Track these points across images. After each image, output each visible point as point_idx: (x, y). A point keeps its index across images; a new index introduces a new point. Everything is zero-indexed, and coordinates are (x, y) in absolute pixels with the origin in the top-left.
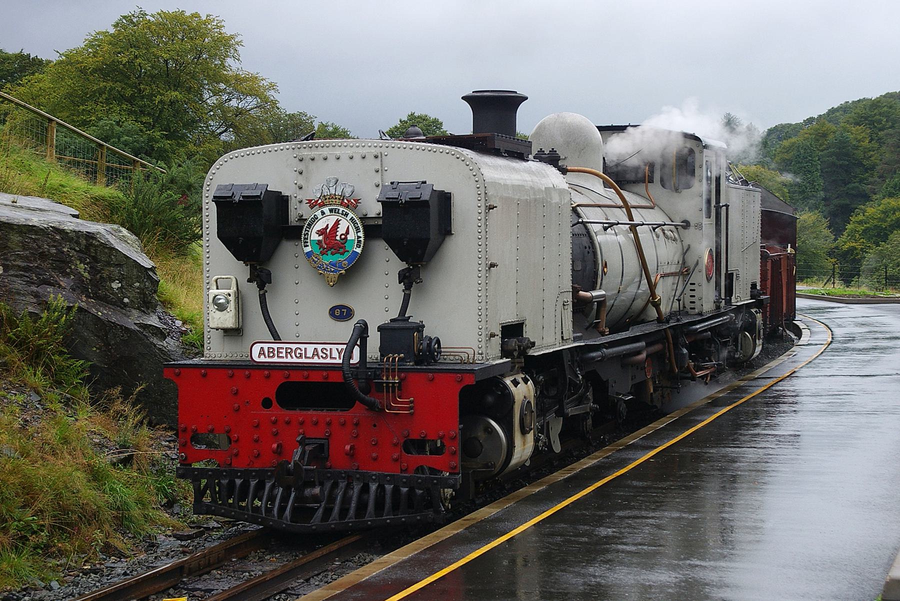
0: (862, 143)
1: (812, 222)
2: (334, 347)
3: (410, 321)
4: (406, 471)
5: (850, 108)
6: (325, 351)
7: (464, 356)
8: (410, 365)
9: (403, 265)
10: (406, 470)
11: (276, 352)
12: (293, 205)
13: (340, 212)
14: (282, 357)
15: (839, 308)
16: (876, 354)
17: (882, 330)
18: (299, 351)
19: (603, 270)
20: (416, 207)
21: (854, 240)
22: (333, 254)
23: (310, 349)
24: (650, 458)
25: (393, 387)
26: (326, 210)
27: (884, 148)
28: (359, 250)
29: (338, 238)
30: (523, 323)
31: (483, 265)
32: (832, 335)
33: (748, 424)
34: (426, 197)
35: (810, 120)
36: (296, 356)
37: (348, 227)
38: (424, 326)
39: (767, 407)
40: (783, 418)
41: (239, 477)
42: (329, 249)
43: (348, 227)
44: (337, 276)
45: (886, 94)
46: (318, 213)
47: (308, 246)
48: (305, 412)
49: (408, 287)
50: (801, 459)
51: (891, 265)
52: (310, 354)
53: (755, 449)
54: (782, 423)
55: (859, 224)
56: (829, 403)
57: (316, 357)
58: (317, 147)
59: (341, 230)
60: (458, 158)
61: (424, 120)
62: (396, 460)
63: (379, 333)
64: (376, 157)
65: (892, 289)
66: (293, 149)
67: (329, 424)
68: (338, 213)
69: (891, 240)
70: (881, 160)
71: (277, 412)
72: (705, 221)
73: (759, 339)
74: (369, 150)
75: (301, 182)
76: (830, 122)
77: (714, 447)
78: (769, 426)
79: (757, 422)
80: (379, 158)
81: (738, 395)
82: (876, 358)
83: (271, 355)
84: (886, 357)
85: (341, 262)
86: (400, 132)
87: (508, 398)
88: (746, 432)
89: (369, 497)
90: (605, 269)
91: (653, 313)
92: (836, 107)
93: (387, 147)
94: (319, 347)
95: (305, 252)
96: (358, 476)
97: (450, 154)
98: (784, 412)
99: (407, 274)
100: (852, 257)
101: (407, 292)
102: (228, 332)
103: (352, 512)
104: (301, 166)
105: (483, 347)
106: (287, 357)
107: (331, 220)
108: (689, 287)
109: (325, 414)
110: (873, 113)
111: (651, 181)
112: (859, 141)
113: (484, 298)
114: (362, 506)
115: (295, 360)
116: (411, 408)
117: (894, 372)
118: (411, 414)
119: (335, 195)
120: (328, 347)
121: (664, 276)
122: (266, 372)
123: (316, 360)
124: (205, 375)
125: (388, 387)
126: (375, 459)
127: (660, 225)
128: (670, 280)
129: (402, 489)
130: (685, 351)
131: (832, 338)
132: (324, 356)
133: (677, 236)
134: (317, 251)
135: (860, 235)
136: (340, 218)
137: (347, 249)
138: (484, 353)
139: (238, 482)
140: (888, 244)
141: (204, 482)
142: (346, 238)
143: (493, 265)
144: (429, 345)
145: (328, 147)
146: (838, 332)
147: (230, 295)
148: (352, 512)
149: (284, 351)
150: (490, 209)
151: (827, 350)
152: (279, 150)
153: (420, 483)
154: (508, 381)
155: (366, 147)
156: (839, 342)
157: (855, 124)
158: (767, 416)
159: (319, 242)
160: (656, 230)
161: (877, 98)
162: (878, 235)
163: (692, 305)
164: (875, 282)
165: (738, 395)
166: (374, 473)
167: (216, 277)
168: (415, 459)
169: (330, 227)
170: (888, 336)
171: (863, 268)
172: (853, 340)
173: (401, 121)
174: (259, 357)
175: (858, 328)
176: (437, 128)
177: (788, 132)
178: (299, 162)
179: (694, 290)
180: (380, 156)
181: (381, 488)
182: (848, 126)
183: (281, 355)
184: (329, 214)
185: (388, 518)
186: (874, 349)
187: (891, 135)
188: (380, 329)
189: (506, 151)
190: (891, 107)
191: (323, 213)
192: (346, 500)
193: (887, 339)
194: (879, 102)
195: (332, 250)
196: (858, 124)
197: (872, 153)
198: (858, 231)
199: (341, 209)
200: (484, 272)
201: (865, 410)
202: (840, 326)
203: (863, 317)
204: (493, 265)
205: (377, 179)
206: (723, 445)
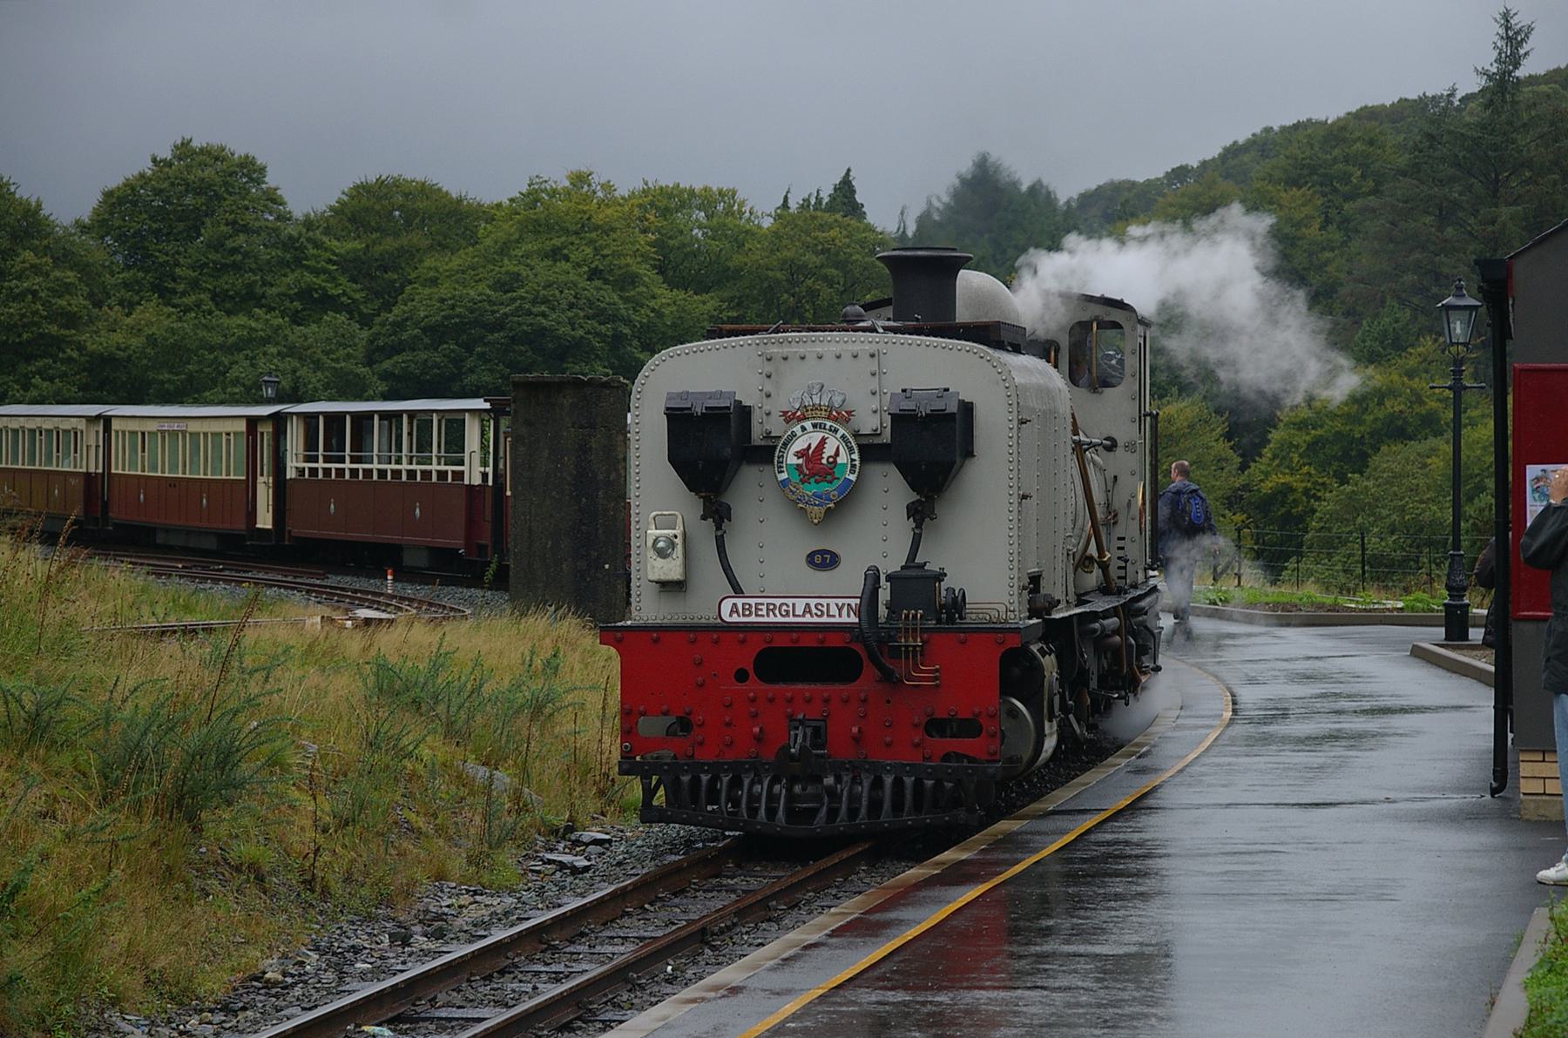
0: (1304, 229)
1: (1185, 424)
4: (930, 759)
6: (820, 607)
8: (932, 623)
9: (914, 497)
11: (753, 609)
12: (756, 418)
13: (827, 427)
14: (763, 616)
15: (1250, 635)
16: (1336, 751)
17: (1354, 691)
18: (784, 607)
20: (939, 419)
21: (1288, 467)
22: (817, 482)
23: (800, 605)
24: (786, 1020)
25: (915, 652)
26: (808, 424)
28: (853, 477)
29: (824, 461)
30: (1040, 576)
31: (1016, 495)
32: (1234, 703)
33: (1028, 929)
35: (1180, 173)
37: (838, 449)
38: (946, 575)
40: (1113, 913)
41: (707, 772)
42: (812, 475)
43: (838, 449)
44: (823, 511)
45: (1361, 109)
46: (797, 429)
49: (919, 525)
50: (1155, 1015)
51: (1375, 530)
52: (799, 611)
53: (1046, 993)
54: (1111, 925)
55: (1300, 429)
56: (1226, 873)
57: (808, 615)
59: (829, 451)
60: (982, 357)
61: (217, 159)
62: (917, 746)
63: (889, 584)
64: (872, 356)
65: (1379, 589)
67: (827, 701)
69: (1375, 469)
70: (1349, 273)
71: (754, 686)
73: (1050, 721)
75: (768, 388)
76: (1227, 176)
77: (946, 988)
78: (1079, 934)
81: (1007, 856)
83: (747, 613)
84: (1361, 758)
85: (828, 493)
86: (154, 189)
88: (1022, 950)
89: (883, 792)
92: (1241, 141)
93: (886, 343)
94: (813, 602)
96: (867, 767)
97: (971, 353)
98: (1118, 897)
101: (917, 531)
102: (666, 586)
104: (769, 368)
105: (1016, 602)
106: (768, 615)
107: (814, 438)
109: (837, 687)
110: (1329, 157)
112: (1298, 225)
114: (875, 806)
115: (780, 619)
116: (936, 678)
117: (1383, 795)
118: (937, 686)
119: (820, 405)
122: (741, 636)
123: (808, 619)
125: (907, 652)
126: (888, 745)
129: (926, 782)
131: (1235, 711)
132: (819, 613)
134: (796, 478)
135: (1301, 456)
136: (827, 436)
137: (836, 475)
140: (1368, 479)
142: (835, 462)
143: (1024, 497)
147: (676, 537)
149: (764, 608)
150: (1023, 423)
151: (1220, 742)
152: (738, 347)
153: (950, 774)
154: (1034, 648)
155: (858, 342)
156: (1251, 721)
157: (1286, 183)
158: (1075, 909)
159: (798, 467)
163: (1122, 573)
164: (1337, 571)
165: (1007, 856)
167: (654, 513)
169: (813, 447)
170: (1366, 705)
172: (1285, 716)
173: (154, 160)
175: (1296, 687)
176: (251, 180)
177: (1127, 201)
178: (766, 362)
180: (876, 353)
181: (898, 783)
182: (1270, 188)
183: (760, 613)
184: (812, 429)
185: (908, 818)
186: (1334, 737)
187: (1374, 210)
189: (1011, 344)
190: (1371, 143)
191: (803, 429)
193: (1365, 712)
195: (817, 477)
196: (1294, 183)
197: (1328, 254)
198: (1297, 447)
199: (829, 424)
201: (1311, 889)
202: (1252, 681)
203: (1309, 658)
204: (1024, 497)
206: (965, 984)
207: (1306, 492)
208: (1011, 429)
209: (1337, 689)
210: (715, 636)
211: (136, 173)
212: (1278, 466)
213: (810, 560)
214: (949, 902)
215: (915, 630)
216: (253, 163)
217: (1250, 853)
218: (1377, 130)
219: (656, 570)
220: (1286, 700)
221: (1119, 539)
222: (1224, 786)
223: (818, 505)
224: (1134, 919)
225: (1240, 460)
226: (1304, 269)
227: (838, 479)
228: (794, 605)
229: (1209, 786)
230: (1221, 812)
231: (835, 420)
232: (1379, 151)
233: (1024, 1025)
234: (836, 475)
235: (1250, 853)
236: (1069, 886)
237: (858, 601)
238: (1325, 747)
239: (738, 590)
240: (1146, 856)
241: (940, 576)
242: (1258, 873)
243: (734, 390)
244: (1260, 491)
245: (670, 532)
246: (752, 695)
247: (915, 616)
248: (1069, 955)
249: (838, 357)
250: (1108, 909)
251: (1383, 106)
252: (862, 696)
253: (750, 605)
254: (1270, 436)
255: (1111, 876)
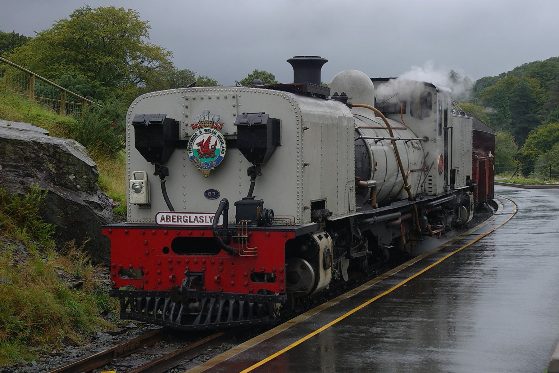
0: (535, 89)
2: (207, 215)
3: (254, 199)
4: (252, 292)
5: (528, 67)
6: (202, 218)
7: (288, 221)
8: (255, 226)
9: (251, 165)
10: (252, 292)
11: (171, 219)
12: (182, 127)
13: (211, 131)
14: (175, 222)
15: (521, 191)
16: (544, 220)
18: (185, 218)
19: (375, 168)
20: (259, 128)
22: (207, 158)
23: (193, 216)
24: (404, 284)
25: (244, 240)
26: (203, 130)
27: (549, 92)
28: (223, 155)
29: (210, 148)
30: (325, 200)
32: (517, 208)
33: (465, 263)
34: (265, 122)
35: (503, 75)
36: (184, 221)
37: (216, 141)
39: (476, 252)
40: (486, 260)
41: (149, 296)
43: (216, 141)
44: (209, 171)
46: (198, 132)
47: (191, 153)
48: (189, 256)
49: (253, 178)
51: (553, 165)
53: (469, 279)
55: (534, 139)
56: (515, 250)
57: (196, 222)
58: (197, 91)
59: (212, 143)
60: (284, 98)
61: (263, 74)
62: (246, 285)
64: (234, 97)
66: (182, 92)
67: (204, 263)
68: (210, 132)
70: (547, 99)
71: (172, 256)
72: (438, 137)
73: (471, 211)
74: (229, 93)
75: (187, 113)
76: (515, 75)
78: (478, 264)
79: (470, 262)
80: (236, 98)
81: (459, 245)
82: (544, 222)
83: (169, 220)
84: (551, 221)
85: (212, 163)
86: (249, 82)
87: (315, 247)
88: (463, 268)
89: (229, 308)
90: (376, 167)
91: (405, 194)
92: (519, 66)
93: (240, 91)
94: (198, 215)
95: (190, 156)
96: (222, 295)
98: (487, 256)
99: (253, 170)
100: (529, 160)
101: (253, 181)
102: (141, 206)
103: (219, 318)
104: (187, 103)
105: (300, 215)
106: (178, 221)
107: (206, 137)
108: (428, 178)
111: (404, 112)
112: (534, 88)
113: (300, 185)
114: (225, 314)
115: (183, 223)
116: (255, 253)
117: (556, 231)
119: (208, 121)
120: (204, 215)
121: (412, 171)
123: (196, 223)
124: (127, 233)
125: (241, 240)
126: (233, 285)
127: (410, 140)
128: (416, 174)
129: (250, 303)
130: (425, 218)
131: (517, 210)
132: (201, 221)
133: (420, 146)
134: (197, 156)
135: (534, 146)
136: (211, 135)
137: (215, 154)
138: (301, 219)
139: (148, 299)
140: (551, 152)
141: (127, 299)
142: (215, 148)
143: (306, 165)
144: (267, 214)
145: (203, 91)
146: (521, 206)
147: (143, 183)
148: (219, 318)
149: (176, 218)
150: (304, 130)
151: (513, 218)
152: (173, 94)
154: (315, 237)
156: (521, 212)
158: (477, 258)
159: (198, 150)
160: (408, 143)
161: (545, 61)
162: (546, 146)
163: (430, 190)
165: (459, 245)
166: (232, 293)
168: (258, 284)
169: (205, 141)
170: (551, 208)
171: (536, 166)
172: (530, 211)
173: (249, 75)
174: (161, 221)
175: (533, 204)
176: (271, 79)
178: (185, 101)
179: (431, 180)
180: (236, 97)
181: (237, 303)
182: (527, 78)
183: (174, 220)
184: (204, 133)
185: (241, 321)
186: (543, 216)
187: (554, 84)
188: (236, 204)
190: (553, 67)
191: (201, 132)
192: (215, 310)
193: (551, 210)
194: (546, 63)
195: (206, 155)
197: (541, 95)
198: (533, 144)
199: (212, 130)
200: (300, 169)
201: (537, 254)
202: (522, 202)
203: (536, 197)
204: (306, 165)
205: (234, 111)
206: (449, 276)
207: (535, 154)
208: (298, 132)
209: (544, 204)
210: (153, 231)
211: (245, 78)
212: (528, 148)
213: (206, 194)
214: (444, 257)
215: (244, 230)
216: (272, 75)
217: (521, 245)
218: (555, 64)
219: (134, 199)
220: (531, 207)
221: (429, 176)
222: (514, 228)
223: (207, 169)
224: (492, 261)
225: (518, 147)
226: (535, 99)
227: (216, 156)
228: (190, 216)
229: (511, 228)
230: (513, 235)
231: (216, 128)
232: (555, 69)
233: (464, 287)
234: (215, 154)
235: (521, 245)
236: (475, 253)
237: (214, 215)
238: (541, 219)
239: (172, 210)
240: (494, 246)
241: (261, 203)
242: (524, 250)
243: (166, 114)
244: (523, 155)
245: (142, 181)
246: (170, 260)
247: (245, 223)
248: (475, 270)
249: (218, 98)
250: (485, 259)
251: (556, 57)
252: (221, 261)
253: (170, 216)
254: (526, 141)
255: (486, 250)
